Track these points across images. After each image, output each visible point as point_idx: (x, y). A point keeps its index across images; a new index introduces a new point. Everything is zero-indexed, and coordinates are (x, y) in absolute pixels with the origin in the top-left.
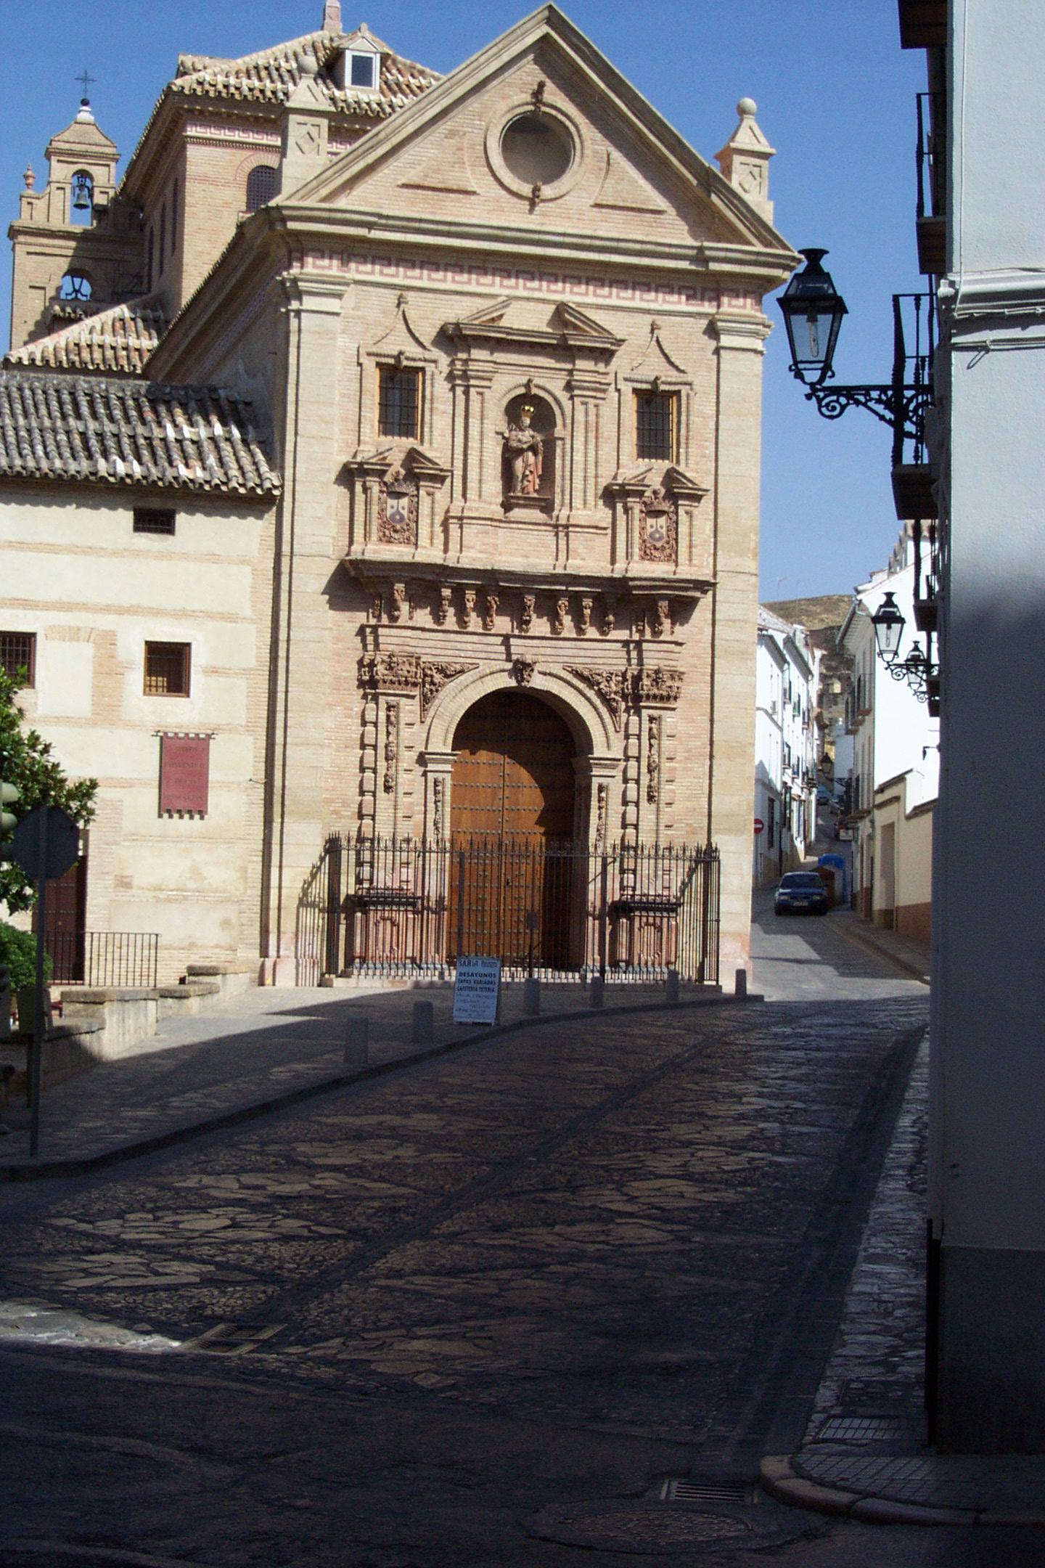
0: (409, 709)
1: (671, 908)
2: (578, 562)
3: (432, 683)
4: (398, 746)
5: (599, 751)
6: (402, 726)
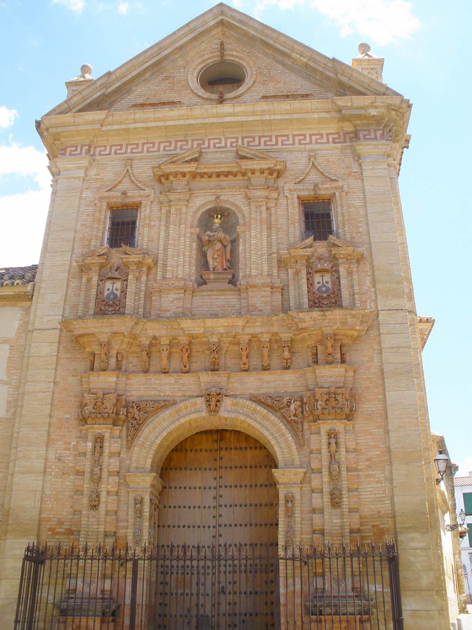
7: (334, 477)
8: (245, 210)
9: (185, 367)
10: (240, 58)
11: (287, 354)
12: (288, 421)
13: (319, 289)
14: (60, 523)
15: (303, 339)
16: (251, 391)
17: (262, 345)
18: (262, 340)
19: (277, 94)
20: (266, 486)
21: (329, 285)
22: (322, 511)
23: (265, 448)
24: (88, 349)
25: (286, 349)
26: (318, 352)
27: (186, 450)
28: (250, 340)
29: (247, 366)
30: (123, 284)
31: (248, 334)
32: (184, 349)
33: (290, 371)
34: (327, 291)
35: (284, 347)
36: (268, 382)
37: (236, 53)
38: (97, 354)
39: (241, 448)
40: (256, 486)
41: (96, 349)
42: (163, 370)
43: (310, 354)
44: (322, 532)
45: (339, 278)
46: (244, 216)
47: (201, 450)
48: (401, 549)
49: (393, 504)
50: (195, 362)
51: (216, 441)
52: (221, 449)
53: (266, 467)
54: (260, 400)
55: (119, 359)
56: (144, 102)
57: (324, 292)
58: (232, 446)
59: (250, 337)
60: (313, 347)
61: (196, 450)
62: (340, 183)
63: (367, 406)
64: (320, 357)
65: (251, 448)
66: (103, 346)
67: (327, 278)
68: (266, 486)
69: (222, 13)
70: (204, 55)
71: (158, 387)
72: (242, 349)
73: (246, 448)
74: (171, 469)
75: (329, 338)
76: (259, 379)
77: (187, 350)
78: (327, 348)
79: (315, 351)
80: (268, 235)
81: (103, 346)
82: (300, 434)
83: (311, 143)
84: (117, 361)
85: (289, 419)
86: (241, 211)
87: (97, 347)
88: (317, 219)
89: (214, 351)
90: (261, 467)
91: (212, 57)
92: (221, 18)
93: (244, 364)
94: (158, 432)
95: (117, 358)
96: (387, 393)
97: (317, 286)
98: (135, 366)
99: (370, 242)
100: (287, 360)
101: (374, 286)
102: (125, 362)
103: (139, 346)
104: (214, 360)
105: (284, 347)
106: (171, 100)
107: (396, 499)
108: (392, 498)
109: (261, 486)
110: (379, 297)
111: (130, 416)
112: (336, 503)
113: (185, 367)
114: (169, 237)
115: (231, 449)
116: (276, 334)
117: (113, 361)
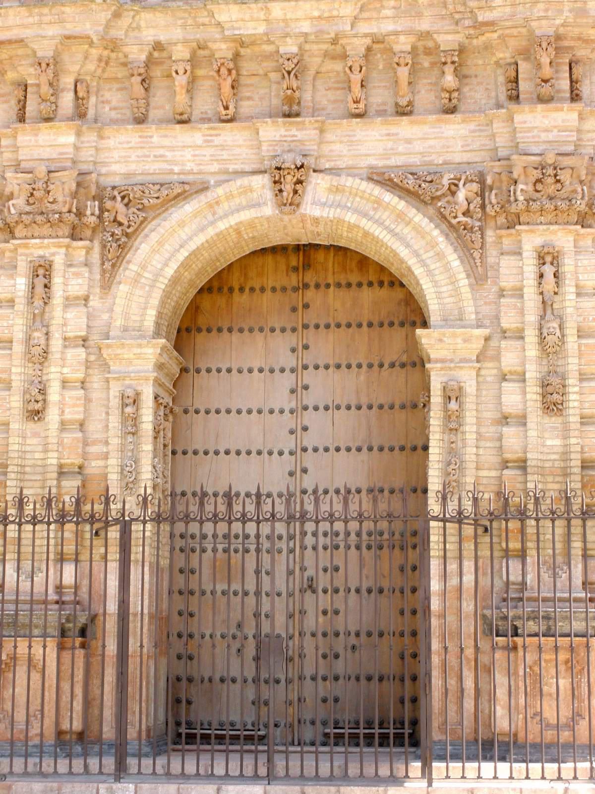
9: (226, 108)
11: (450, 80)
12: (451, 226)
15: (487, 47)
16: (372, 161)
17: (396, 60)
18: (397, 48)
20: (403, 365)
23: (402, 285)
24: (11, 75)
25: (449, 69)
26: (520, 76)
27: (231, 290)
28: (369, 49)
29: (361, 106)
31: (366, 35)
32: (224, 71)
33: (457, 117)
35: (445, 63)
36: (409, 141)
38: (32, 85)
39: (349, 285)
40: (381, 366)
41: (29, 73)
42: (178, 117)
43: (501, 79)
47: (263, 290)
50: (249, 98)
51: (296, 269)
52: (306, 286)
53: (402, 324)
54: (391, 180)
55: (80, 94)
58: (331, 281)
59: (368, 41)
60: (510, 64)
61: (252, 289)
64: (523, 86)
65: (370, 284)
66: (44, 65)
68: (403, 365)
71: (167, 154)
72: (350, 68)
73: (360, 285)
74: (199, 330)
75: (544, 45)
76: (388, 135)
77: (230, 71)
78: (539, 66)
79: (514, 74)
81: (44, 65)
82: (477, 255)
84: (77, 97)
85: (454, 221)
87: (31, 70)
89: (289, 73)
90: (391, 324)
93: (356, 102)
95: (76, 92)
98: (115, 109)
100: (450, 92)
102: (93, 100)
103: (125, 65)
104: (289, 92)
105: (445, 63)
109: (392, 365)
113: (226, 108)
115: (328, 286)
116: (427, 35)
117: (67, 100)
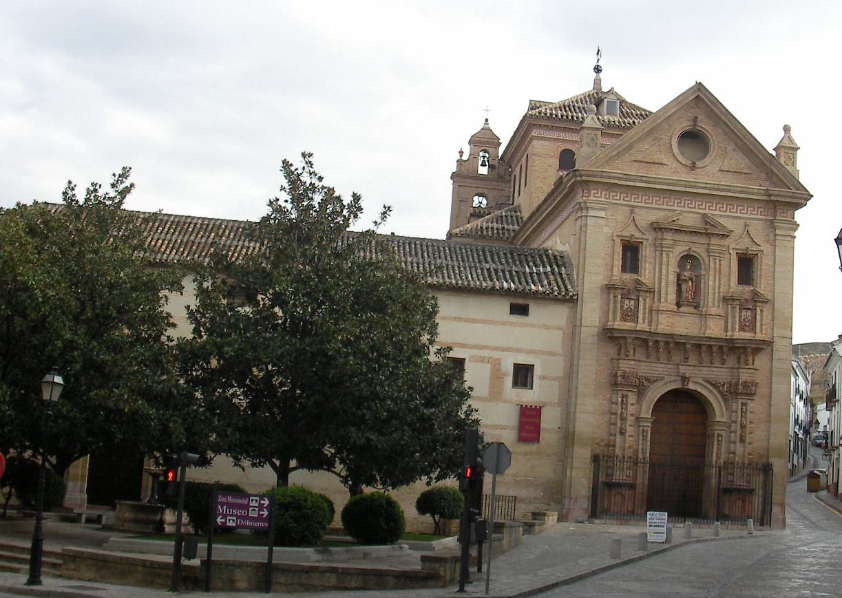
0: (632, 398)
1: (751, 492)
2: (662, 327)
3: (643, 385)
4: (626, 414)
5: (718, 419)
6: (629, 405)
7: (743, 427)
8: (706, 259)
10: (707, 131)
13: (744, 319)
14: (602, 440)
19: (729, 170)
21: (750, 318)
22: (735, 443)
30: (635, 302)
34: (748, 321)
37: (705, 126)
44: (734, 453)
45: (756, 314)
46: (705, 264)
48: (553, 354)
49: (769, 443)
56: (641, 160)
57: (747, 322)
62: (762, 248)
63: (762, 390)
67: (749, 313)
69: (699, 90)
70: (684, 125)
80: (721, 278)
83: (747, 213)
86: (704, 260)
88: (746, 264)
91: (688, 126)
92: (698, 93)
94: (655, 393)
96: (773, 385)
97: (743, 317)
99: (769, 415)
101: (773, 320)
106: (660, 161)
107: (771, 441)
108: (768, 440)
110: (775, 328)
111: (641, 386)
112: (742, 440)
114: (660, 270)
